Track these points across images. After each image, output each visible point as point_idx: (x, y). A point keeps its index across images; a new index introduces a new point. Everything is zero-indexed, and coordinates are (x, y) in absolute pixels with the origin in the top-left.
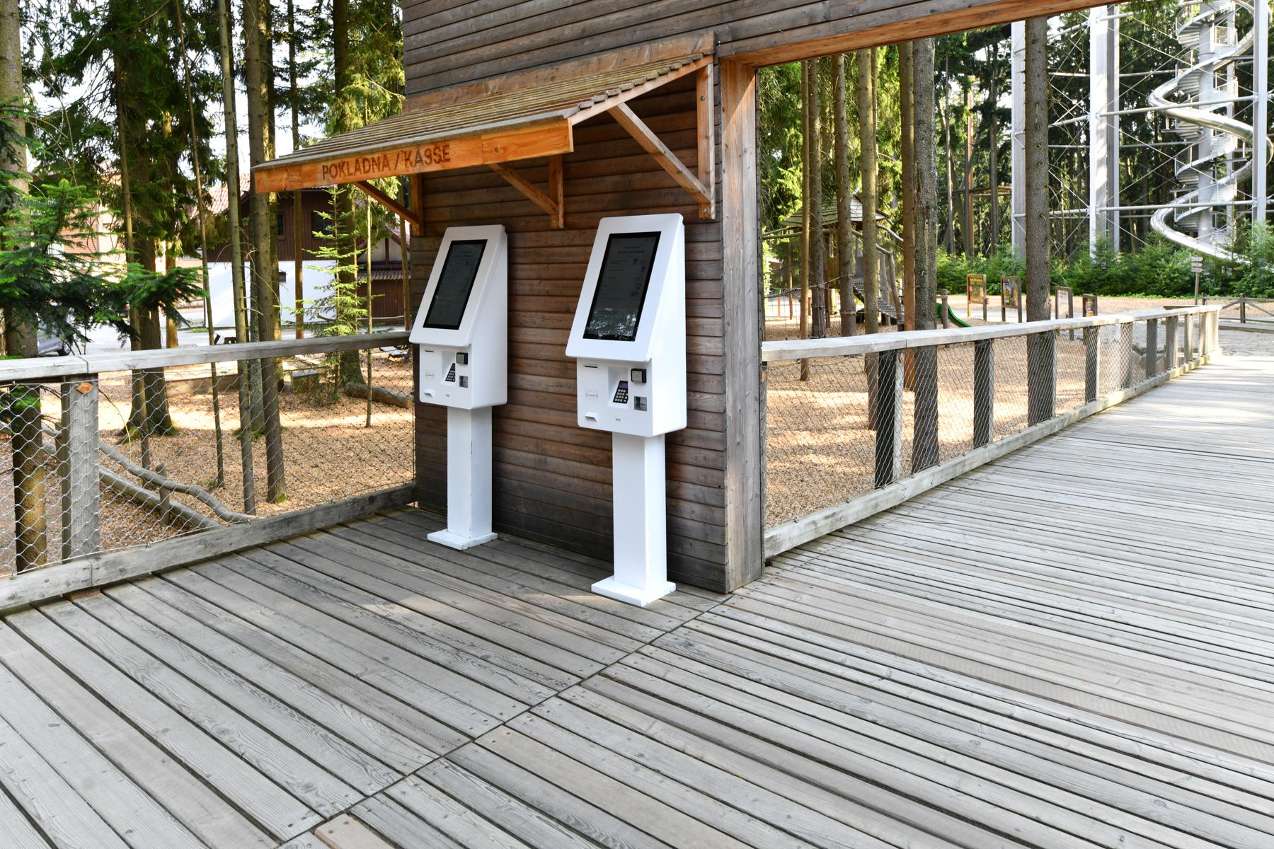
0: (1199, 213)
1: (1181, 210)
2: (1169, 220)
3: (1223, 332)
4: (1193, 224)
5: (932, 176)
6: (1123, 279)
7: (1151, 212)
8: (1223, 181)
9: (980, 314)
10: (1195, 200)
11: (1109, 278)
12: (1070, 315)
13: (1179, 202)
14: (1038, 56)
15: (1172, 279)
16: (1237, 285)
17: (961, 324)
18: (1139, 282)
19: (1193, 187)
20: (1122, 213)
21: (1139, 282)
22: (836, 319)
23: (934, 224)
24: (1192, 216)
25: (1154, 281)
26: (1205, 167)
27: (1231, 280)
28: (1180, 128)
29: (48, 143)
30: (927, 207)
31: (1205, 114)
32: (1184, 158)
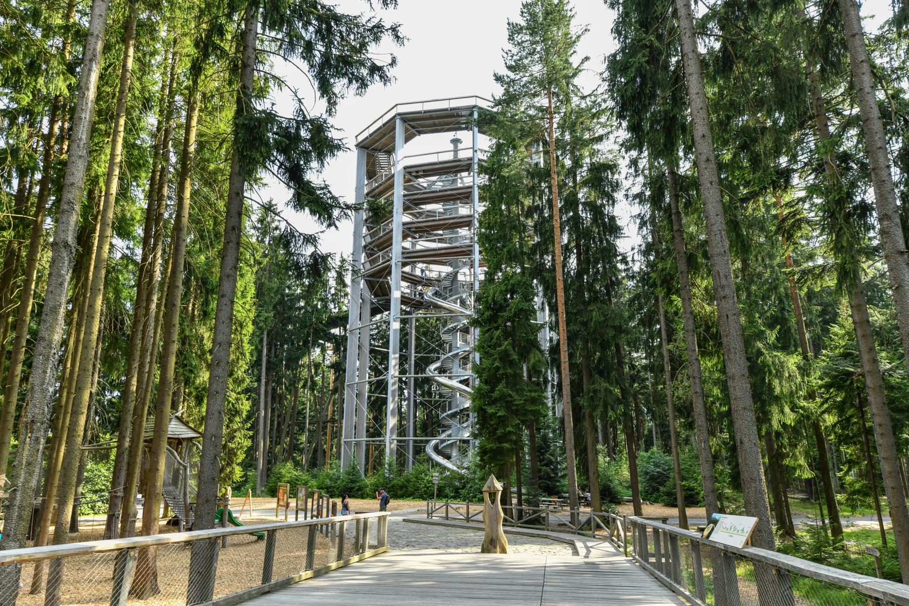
0: (452, 444)
1: (443, 441)
2: (436, 449)
3: (355, 522)
4: (448, 451)
5: (44, 391)
6: (401, 487)
7: (427, 442)
8: (465, 425)
9: (283, 518)
10: (450, 436)
11: (393, 486)
12: (319, 514)
13: (443, 436)
14: (224, 307)
15: (428, 488)
16: (462, 492)
17: (237, 525)
18: (410, 489)
19: (449, 427)
20: (415, 441)
21: (410, 489)
22: (139, 524)
23: (37, 440)
24: (448, 445)
25: (417, 489)
26: (453, 416)
27: (459, 489)
28: (445, 391)
29: (647, 172)
30: (33, 421)
31: (454, 383)
32: (444, 411)
